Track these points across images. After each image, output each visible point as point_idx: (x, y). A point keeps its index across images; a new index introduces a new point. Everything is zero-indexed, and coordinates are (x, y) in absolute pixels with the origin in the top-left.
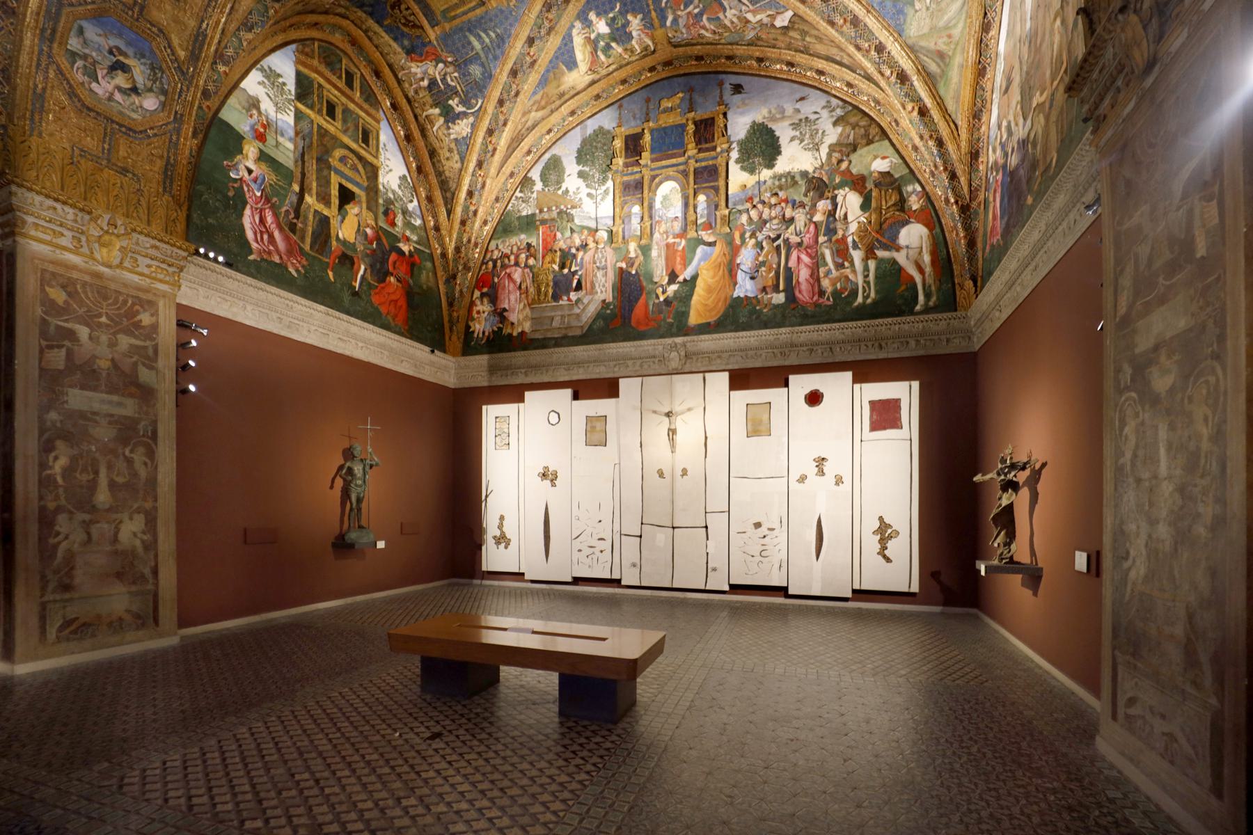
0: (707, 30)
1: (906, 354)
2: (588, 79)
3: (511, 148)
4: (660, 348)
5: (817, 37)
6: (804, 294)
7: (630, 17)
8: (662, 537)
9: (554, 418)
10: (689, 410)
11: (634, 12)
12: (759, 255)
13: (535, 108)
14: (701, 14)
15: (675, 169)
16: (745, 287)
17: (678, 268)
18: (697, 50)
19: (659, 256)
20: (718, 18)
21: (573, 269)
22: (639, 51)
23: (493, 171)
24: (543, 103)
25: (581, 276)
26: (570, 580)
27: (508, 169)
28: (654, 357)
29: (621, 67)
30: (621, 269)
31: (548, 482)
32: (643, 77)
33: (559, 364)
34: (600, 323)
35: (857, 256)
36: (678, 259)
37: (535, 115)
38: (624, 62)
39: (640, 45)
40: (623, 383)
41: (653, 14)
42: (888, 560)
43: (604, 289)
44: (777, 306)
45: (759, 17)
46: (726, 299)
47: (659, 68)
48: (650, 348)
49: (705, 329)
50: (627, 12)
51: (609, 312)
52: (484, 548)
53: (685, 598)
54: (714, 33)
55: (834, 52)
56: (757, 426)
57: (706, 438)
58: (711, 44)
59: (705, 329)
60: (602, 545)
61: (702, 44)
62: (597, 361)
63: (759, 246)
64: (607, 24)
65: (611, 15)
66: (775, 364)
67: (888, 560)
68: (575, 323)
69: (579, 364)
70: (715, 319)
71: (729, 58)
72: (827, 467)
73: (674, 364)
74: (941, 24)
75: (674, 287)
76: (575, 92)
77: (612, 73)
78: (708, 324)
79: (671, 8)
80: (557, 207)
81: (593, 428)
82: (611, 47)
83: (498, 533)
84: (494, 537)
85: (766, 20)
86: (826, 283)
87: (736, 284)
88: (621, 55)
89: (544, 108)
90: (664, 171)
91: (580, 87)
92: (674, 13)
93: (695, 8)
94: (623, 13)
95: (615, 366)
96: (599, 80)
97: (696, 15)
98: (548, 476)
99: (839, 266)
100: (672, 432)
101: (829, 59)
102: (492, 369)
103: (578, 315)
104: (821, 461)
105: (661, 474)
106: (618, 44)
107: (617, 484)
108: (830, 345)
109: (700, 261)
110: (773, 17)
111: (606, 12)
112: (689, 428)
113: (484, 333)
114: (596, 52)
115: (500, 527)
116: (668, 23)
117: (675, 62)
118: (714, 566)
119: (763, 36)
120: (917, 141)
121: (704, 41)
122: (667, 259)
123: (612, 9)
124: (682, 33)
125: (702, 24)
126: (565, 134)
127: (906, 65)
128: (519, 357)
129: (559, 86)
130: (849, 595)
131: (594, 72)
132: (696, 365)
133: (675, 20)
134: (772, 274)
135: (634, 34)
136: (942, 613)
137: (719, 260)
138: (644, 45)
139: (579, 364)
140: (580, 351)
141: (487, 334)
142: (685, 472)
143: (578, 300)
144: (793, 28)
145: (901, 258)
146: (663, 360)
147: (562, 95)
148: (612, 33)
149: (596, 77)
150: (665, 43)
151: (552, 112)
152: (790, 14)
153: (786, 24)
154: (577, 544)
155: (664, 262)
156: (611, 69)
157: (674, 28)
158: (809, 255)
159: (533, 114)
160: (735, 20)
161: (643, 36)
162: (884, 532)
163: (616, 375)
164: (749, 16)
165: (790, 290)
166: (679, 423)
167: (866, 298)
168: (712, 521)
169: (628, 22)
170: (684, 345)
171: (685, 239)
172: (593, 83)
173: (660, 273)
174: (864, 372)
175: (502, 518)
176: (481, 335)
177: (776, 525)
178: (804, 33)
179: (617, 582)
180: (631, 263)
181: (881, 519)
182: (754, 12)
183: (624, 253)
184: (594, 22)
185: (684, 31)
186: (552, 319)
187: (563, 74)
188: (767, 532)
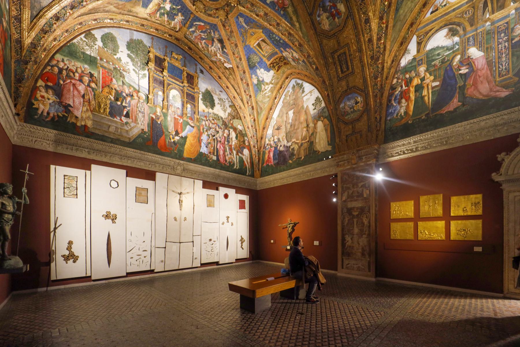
0: (201, 44)
1: (245, 187)
2: (146, 16)
3: (90, 12)
4: (173, 163)
5: (234, 78)
6: (221, 159)
7: (180, 14)
8: (175, 247)
9: (114, 184)
10: (188, 193)
11: (183, 15)
12: (208, 139)
13: (115, 5)
14: (204, 39)
15: (179, 87)
16: (204, 150)
17: (179, 130)
18: (192, 46)
19: (171, 121)
20: (208, 46)
21: (124, 104)
22: (172, 26)
23: (75, 15)
24: (120, 7)
25: (129, 110)
26: (125, 274)
27: (81, 19)
28: (170, 166)
29: (161, 24)
30: (152, 118)
31: (110, 221)
32: (165, 35)
33: (114, 154)
34: (140, 140)
35: (235, 152)
36: (179, 127)
37: (112, 8)
38: (163, 24)
39: (174, 25)
40: (158, 175)
41: (189, 23)
42: (243, 249)
43: (143, 124)
44: (214, 161)
45: (221, 58)
46: (197, 151)
47: (173, 38)
48: (168, 161)
49: (190, 160)
50: (180, 12)
51: (145, 136)
52: (53, 265)
53: (183, 273)
54: (203, 48)
55: (236, 86)
56: (210, 204)
57: (194, 205)
58: (199, 49)
59: (190, 160)
60: (145, 254)
61: (195, 46)
62: (140, 160)
63: (208, 135)
64: (170, 8)
65: (174, 7)
66: (213, 181)
67: (243, 249)
68: (125, 134)
69: (129, 158)
70: (194, 157)
71: (201, 58)
72: (230, 220)
73: (178, 172)
74: (264, 101)
75: (177, 138)
76: (136, 15)
77: (156, 23)
78: (191, 159)
79: (196, 27)
80: (113, 64)
81: (140, 194)
82: (164, 15)
83: (67, 253)
84: (63, 256)
85: (222, 60)
86: (227, 158)
87: (201, 147)
88: (165, 21)
89: (118, 9)
90: (173, 84)
91: (140, 15)
92: (196, 29)
93: (204, 35)
94: (179, 11)
95: (149, 164)
96: (149, 21)
97: (202, 38)
98: (109, 216)
99: (230, 154)
100: (180, 201)
101: (233, 86)
102: (57, 142)
103: (127, 131)
104: (228, 217)
105: (175, 219)
106: (167, 17)
107: (153, 222)
108: (228, 179)
109: (188, 131)
110: (225, 62)
111: (174, 4)
112: (187, 200)
113: (48, 113)
114: (158, 11)
115: (69, 248)
116: (191, 30)
117: (181, 42)
118: (196, 257)
119: (218, 64)
120: (250, 126)
121: (197, 46)
122: (175, 124)
123: (177, 6)
124: (192, 37)
125: (201, 41)
126: (119, 27)
127: (254, 105)
128: (72, 138)
129: (132, 7)
130: (199, 265)
131: (150, 16)
132: (193, 175)
133: (194, 32)
134: (212, 148)
135: (176, 20)
136: (253, 263)
137: (195, 134)
138: (175, 27)
139: (129, 158)
140: (130, 151)
141: (52, 115)
142: (185, 219)
143: (127, 123)
144: (229, 70)
145: (244, 157)
146: (173, 168)
147: (130, 11)
148: (169, 12)
149: (149, 18)
150: (183, 33)
151: (120, 13)
152: (231, 66)
153: (228, 67)
154: (129, 255)
155: (173, 125)
156: (157, 21)
157: (191, 33)
158: (223, 147)
159: (112, 7)
160: (213, 51)
161: (178, 24)
162: (242, 240)
163: (155, 170)
164: (218, 55)
165: (218, 156)
166: (183, 197)
167: (237, 167)
168: (196, 239)
169: (177, 15)
170: (183, 164)
171: (183, 119)
172: (146, 19)
173: (171, 128)
174: (239, 190)
175: (70, 243)
176: (45, 114)
177: (216, 240)
178: (231, 74)
179: (152, 271)
180: (157, 116)
181: (241, 236)
182: (221, 55)
183: (154, 111)
184: (167, 2)
185: (193, 37)
186: (109, 126)
187: (139, 5)
188: (213, 242)
